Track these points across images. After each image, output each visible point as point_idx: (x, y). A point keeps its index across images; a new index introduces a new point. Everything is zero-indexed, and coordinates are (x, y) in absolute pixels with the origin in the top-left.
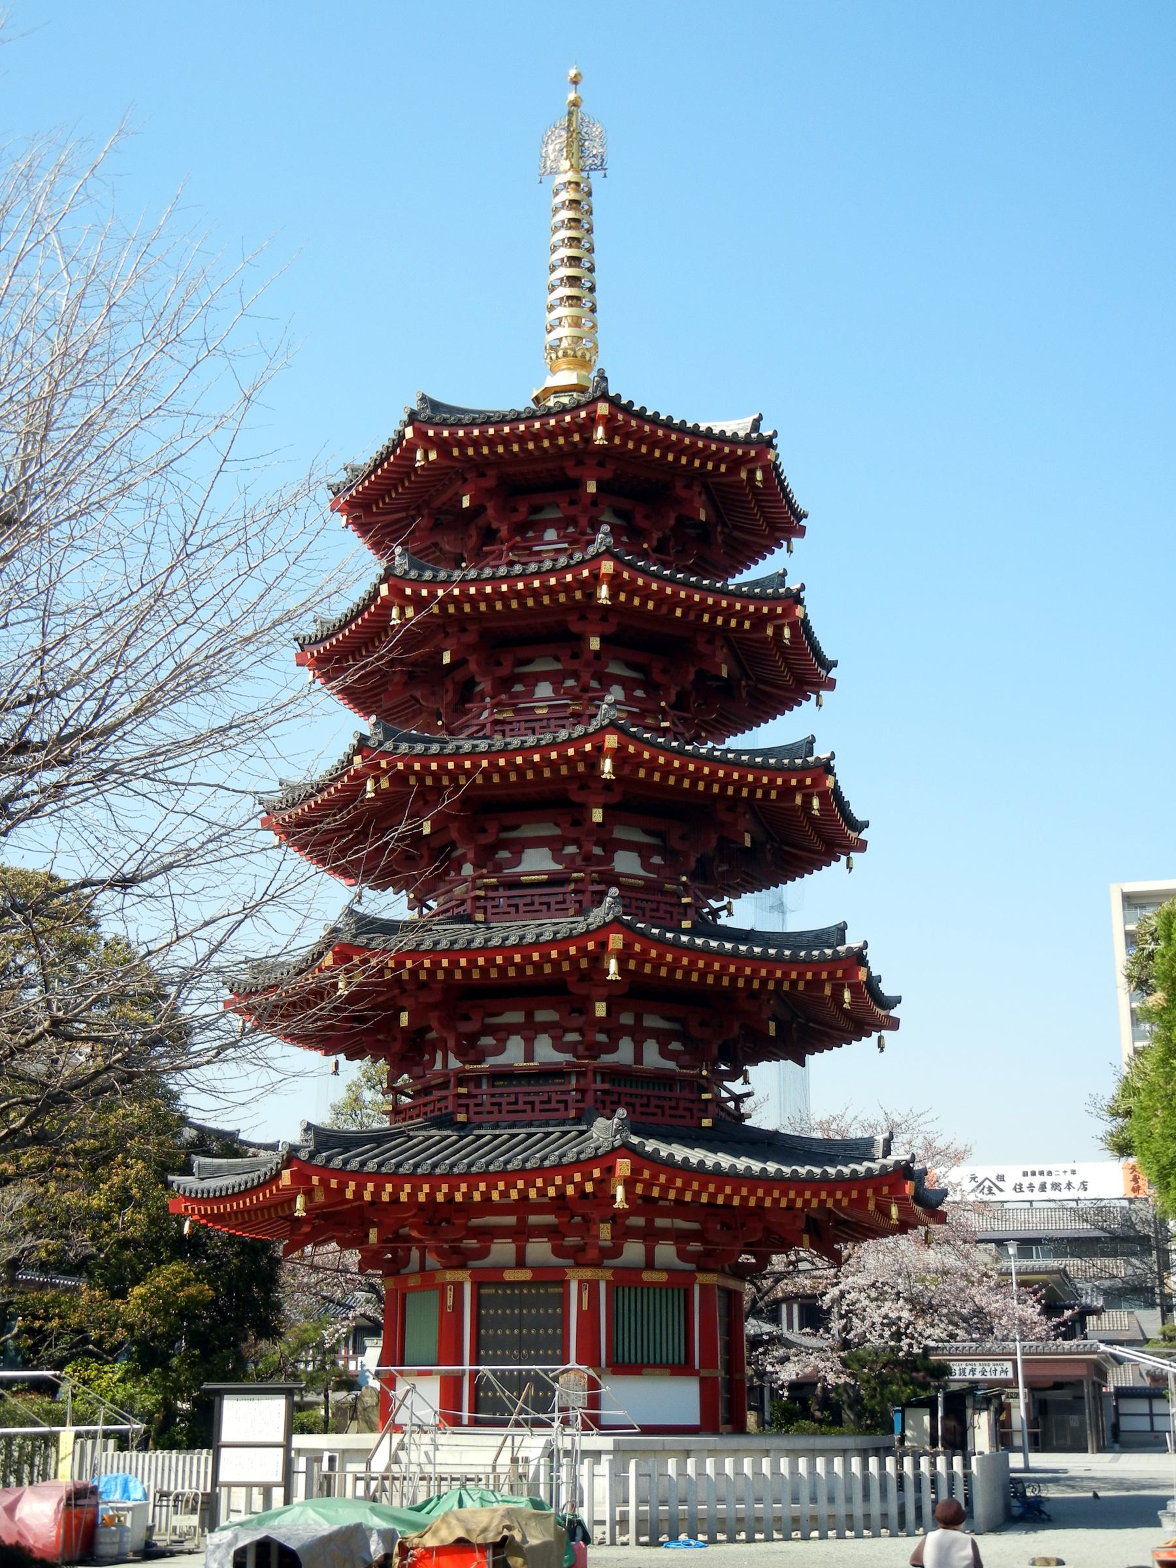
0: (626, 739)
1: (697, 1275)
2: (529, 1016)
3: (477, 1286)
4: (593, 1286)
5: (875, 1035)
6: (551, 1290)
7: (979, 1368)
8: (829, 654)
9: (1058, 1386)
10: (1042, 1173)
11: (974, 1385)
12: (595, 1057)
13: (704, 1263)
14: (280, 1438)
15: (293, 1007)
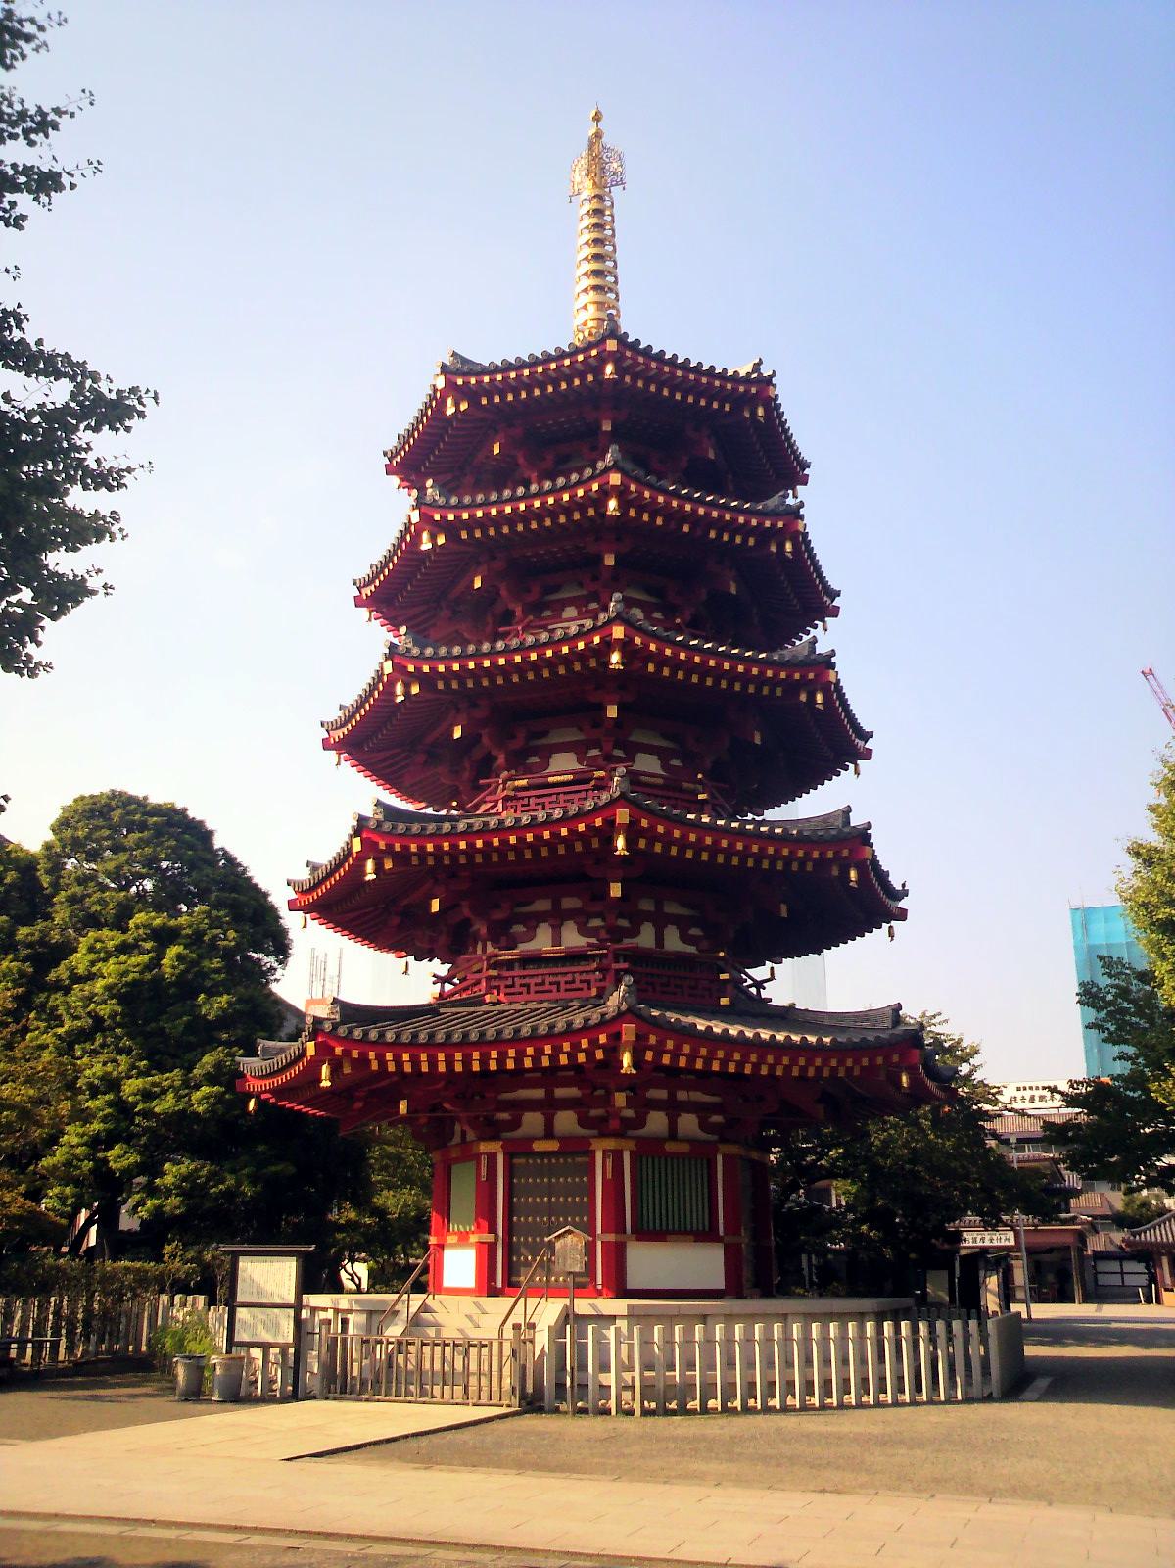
0: (632, 632)
1: (720, 1146)
2: (556, 904)
3: (509, 1157)
4: (617, 1156)
5: (885, 926)
6: (579, 1160)
7: (987, 1237)
8: (834, 584)
9: (1050, 1250)
10: (1031, 1088)
11: (985, 1250)
12: (619, 941)
13: (724, 1134)
14: (291, 1299)
15: (346, 900)
